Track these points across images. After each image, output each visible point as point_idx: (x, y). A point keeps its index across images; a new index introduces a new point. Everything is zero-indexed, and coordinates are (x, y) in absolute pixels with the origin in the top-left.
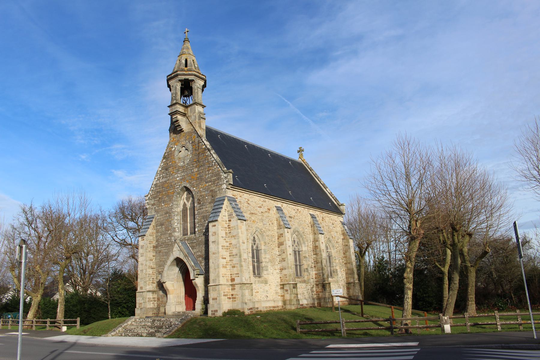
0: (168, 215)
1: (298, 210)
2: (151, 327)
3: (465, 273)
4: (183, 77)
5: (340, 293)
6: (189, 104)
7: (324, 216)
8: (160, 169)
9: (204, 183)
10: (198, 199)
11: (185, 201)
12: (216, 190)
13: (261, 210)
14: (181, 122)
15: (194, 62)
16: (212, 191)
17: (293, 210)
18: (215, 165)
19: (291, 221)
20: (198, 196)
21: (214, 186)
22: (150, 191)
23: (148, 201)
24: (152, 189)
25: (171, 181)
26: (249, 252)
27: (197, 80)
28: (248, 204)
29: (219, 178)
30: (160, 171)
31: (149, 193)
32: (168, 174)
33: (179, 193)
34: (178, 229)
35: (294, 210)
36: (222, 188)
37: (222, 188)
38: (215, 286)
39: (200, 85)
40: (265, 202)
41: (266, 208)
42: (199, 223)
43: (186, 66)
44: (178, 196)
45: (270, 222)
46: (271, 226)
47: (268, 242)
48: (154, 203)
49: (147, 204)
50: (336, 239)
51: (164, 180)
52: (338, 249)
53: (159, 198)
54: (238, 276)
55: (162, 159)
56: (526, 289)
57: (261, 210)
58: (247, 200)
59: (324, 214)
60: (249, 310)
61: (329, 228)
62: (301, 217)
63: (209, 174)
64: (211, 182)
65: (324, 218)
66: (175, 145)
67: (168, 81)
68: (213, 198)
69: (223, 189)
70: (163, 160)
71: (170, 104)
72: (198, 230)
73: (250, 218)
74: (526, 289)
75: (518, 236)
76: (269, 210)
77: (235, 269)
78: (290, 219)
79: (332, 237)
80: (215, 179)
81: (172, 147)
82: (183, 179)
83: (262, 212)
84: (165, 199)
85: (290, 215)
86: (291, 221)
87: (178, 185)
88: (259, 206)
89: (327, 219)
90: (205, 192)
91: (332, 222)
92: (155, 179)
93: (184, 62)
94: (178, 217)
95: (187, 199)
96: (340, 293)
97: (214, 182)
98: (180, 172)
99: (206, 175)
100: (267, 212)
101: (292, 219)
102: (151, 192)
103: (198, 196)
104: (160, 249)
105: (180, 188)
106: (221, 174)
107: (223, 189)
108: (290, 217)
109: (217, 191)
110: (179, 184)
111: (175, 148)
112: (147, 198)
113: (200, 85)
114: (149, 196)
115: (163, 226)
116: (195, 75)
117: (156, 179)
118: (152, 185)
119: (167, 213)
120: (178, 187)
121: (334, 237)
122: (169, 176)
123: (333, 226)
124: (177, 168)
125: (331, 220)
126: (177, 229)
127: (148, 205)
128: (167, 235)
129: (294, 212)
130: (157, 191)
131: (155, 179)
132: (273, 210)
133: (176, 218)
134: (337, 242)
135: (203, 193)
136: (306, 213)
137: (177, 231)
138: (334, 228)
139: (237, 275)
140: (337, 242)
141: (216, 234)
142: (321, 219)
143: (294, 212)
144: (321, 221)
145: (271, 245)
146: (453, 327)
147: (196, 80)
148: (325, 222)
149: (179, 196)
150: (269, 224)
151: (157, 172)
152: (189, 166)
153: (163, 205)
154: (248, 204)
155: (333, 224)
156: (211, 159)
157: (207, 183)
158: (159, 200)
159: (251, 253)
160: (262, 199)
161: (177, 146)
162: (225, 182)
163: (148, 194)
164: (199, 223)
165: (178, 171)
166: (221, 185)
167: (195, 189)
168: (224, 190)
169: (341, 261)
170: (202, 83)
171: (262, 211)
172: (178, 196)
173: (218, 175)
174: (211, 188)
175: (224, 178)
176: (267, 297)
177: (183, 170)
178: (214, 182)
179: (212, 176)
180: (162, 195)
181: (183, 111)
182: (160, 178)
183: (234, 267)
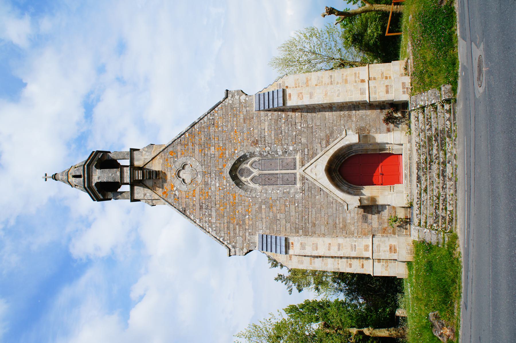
3: (491, 289)
12: (245, 113)
16: (244, 120)
36: (244, 101)
37: (244, 101)
38: (370, 89)
43: (80, 176)
54: (359, 73)
75: (320, 111)
77: (349, 78)
106: (227, 104)
114: (230, 246)
120: (228, 185)
126: (285, 191)
137: (288, 190)
139: (357, 75)
141: (301, 93)
156: (205, 122)
166: (240, 103)
168: (247, 99)
183: (346, 81)
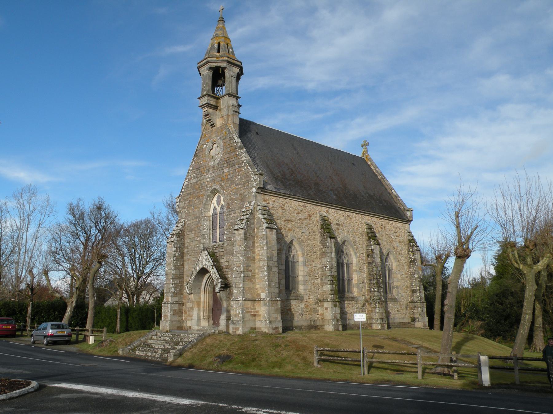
0: (197, 220)
1: (348, 216)
2: (168, 342)
4: (214, 65)
5: (363, 319)
6: (222, 95)
7: (384, 223)
8: (191, 168)
9: (234, 185)
10: (227, 204)
11: (216, 204)
13: (300, 216)
14: (212, 116)
15: (228, 46)
16: (241, 194)
17: (342, 216)
18: (245, 166)
19: (338, 229)
20: (227, 199)
21: (243, 190)
22: (181, 192)
23: (178, 204)
24: (183, 190)
25: (202, 182)
26: (282, 264)
27: (231, 67)
28: (283, 209)
29: (249, 181)
30: (191, 170)
31: (180, 194)
32: (198, 175)
33: (209, 196)
34: (207, 236)
35: (343, 216)
39: (234, 73)
40: (306, 207)
41: (306, 214)
42: (228, 231)
44: (208, 199)
45: (310, 230)
46: (312, 235)
47: (307, 253)
48: (184, 206)
49: (177, 207)
50: (399, 250)
51: (195, 180)
52: (401, 261)
53: (190, 201)
55: (193, 157)
56: (154, 397)
57: (300, 216)
58: (282, 205)
59: (383, 220)
60: (274, 329)
61: (389, 237)
62: (353, 224)
63: (239, 175)
64: (241, 184)
65: (384, 225)
66: (206, 142)
67: (198, 69)
68: (242, 203)
69: (253, 192)
70: (194, 158)
71: (200, 96)
72: (226, 238)
73: (285, 225)
74: (154, 397)
76: (310, 216)
78: (338, 227)
79: (394, 248)
80: (245, 181)
81: (203, 144)
82: (213, 180)
83: (300, 219)
84: (196, 202)
85: (338, 222)
86: (338, 229)
87: (208, 187)
88: (297, 211)
89: (388, 227)
90: (234, 195)
91: (394, 230)
92: (186, 179)
93: (216, 46)
94: (208, 222)
95: (217, 203)
96: (363, 319)
97: (244, 184)
98: (210, 172)
99: (236, 176)
100: (307, 218)
101: (340, 227)
102: (181, 194)
103: (227, 199)
104: (188, 257)
105: (210, 190)
107: (253, 192)
108: (338, 224)
109: (246, 195)
110: (209, 185)
111: (207, 145)
112: (178, 200)
113: (234, 73)
115: (193, 232)
116: (228, 62)
117: (187, 180)
118: (183, 185)
119: (197, 217)
121: (395, 247)
122: (200, 177)
123: (395, 234)
124: (208, 168)
125: (394, 227)
126: (206, 235)
127: (179, 208)
128: (196, 243)
129: (343, 219)
130: (187, 192)
131: (186, 179)
132: (316, 217)
133: (205, 223)
134: (400, 254)
135: (233, 197)
136: (359, 219)
137: (207, 237)
138: (396, 237)
140: (400, 254)
142: (379, 226)
143: (343, 219)
144: (380, 229)
145: (311, 257)
146: (498, 372)
147: (229, 67)
148: (385, 230)
149: (210, 199)
150: (310, 233)
151: (188, 172)
152: (219, 166)
153: (193, 208)
154: (283, 209)
155: (395, 232)
157: (236, 185)
158: (189, 203)
159: (284, 266)
160: (302, 204)
161: (208, 143)
162: (254, 185)
163: (179, 196)
164: (228, 231)
165: (209, 171)
167: (224, 191)
169: (404, 276)
170: (237, 70)
171: (301, 218)
172: (208, 199)
173: (248, 177)
174: (241, 192)
175: (254, 180)
176: (302, 315)
177: (214, 170)
178: (244, 184)
179: (241, 179)
180: (192, 197)
181: (214, 104)
182: (191, 178)
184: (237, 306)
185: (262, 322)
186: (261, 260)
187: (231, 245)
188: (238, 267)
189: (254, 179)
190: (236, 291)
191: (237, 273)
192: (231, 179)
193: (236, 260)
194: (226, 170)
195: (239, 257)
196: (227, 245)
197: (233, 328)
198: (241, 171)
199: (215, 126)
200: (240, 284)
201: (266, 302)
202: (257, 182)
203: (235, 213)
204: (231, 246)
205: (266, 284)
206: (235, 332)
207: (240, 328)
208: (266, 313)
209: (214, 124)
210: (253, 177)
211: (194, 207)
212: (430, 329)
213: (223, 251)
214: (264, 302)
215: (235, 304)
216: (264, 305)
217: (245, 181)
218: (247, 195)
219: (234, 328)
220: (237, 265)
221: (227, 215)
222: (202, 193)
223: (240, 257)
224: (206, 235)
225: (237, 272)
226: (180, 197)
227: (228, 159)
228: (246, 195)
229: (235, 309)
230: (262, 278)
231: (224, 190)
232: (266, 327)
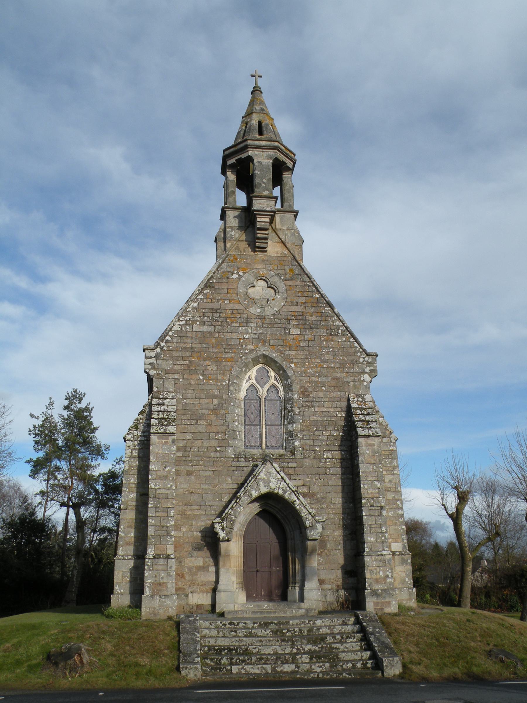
4: (282, 157)
42: (305, 433)
44: (244, 369)
72: (301, 446)
87: (246, 349)
110: (251, 347)
126: (238, 433)
164: (305, 433)
184: (380, 564)
185: (401, 591)
186: (388, 491)
187: (313, 459)
188: (373, 498)
189: (364, 361)
190: (372, 539)
191: (372, 508)
192: (310, 349)
193: (365, 486)
194: (295, 332)
195: (372, 482)
196: (304, 457)
197: (376, 604)
198: (333, 341)
199: (266, 251)
200: (381, 527)
201: (406, 558)
202: (371, 366)
203: (323, 407)
204: (315, 461)
205: (403, 529)
206: (382, 609)
207: (394, 602)
208: (407, 575)
209: (265, 248)
210: (364, 358)
211: (203, 375)
212: (77, 604)
213: (295, 467)
214: (402, 558)
215: (376, 561)
216: (402, 563)
217: (344, 359)
218: (352, 383)
219: (378, 603)
220: (370, 496)
221: (303, 406)
222: (228, 356)
223: (376, 483)
224: (238, 433)
225: (371, 506)
226: (158, 350)
227: (301, 314)
228: (349, 382)
229: (376, 569)
230: (392, 519)
231: (292, 363)
232: (410, 599)
